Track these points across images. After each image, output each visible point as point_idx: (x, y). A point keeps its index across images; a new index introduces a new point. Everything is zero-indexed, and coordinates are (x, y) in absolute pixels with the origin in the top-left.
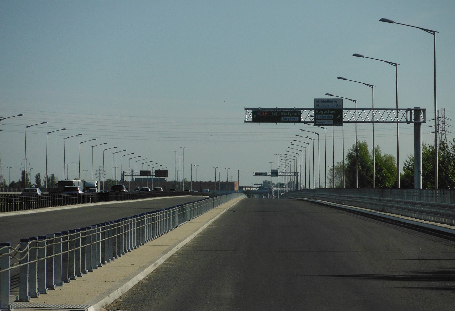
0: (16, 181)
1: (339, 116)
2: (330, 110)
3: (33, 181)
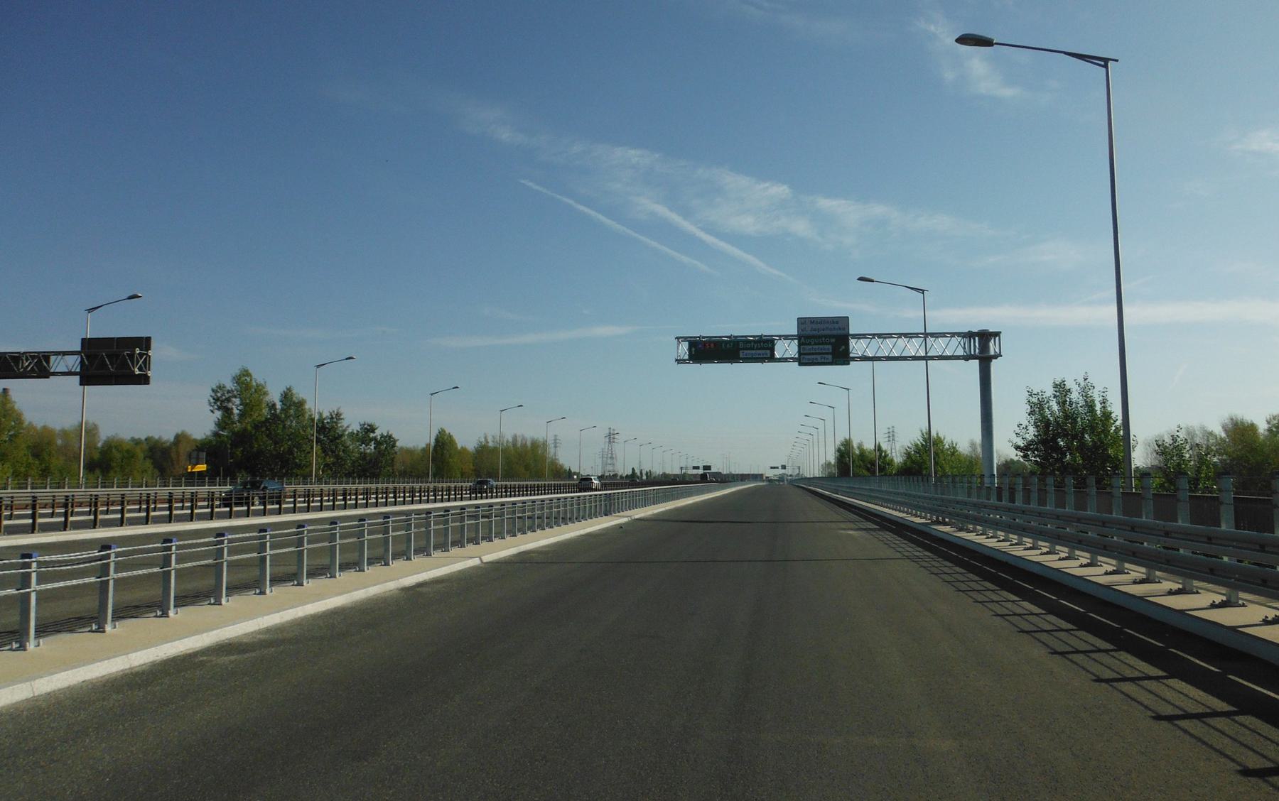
1: (843, 347)
2: (826, 337)
3: (639, 474)
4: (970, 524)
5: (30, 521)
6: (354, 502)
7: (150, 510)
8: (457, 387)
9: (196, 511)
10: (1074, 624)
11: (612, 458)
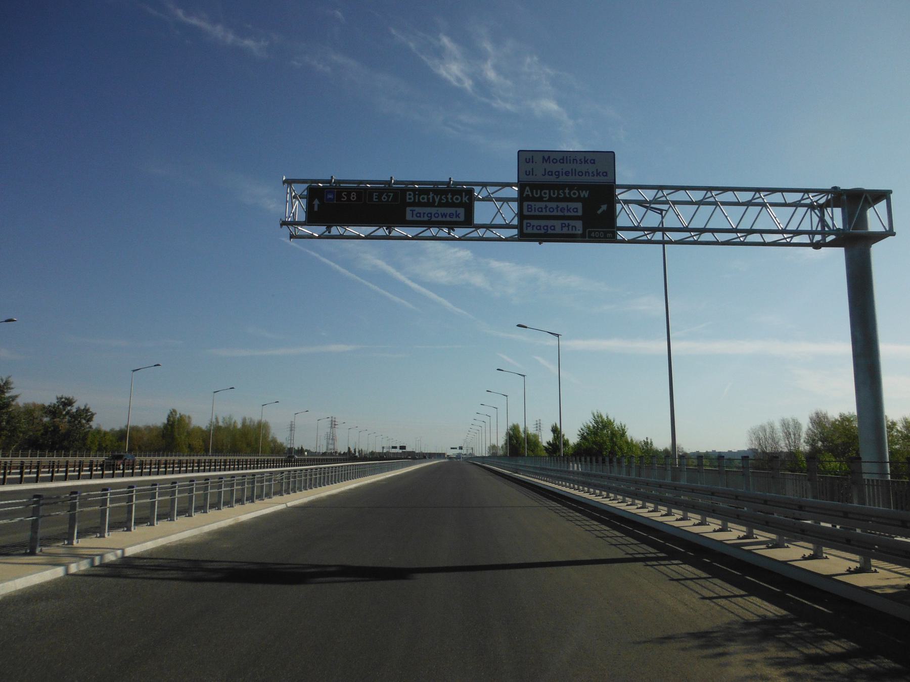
0: (346, 452)
1: (604, 207)
2: (571, 187)
3: (353, 452)
4: (592, 488)
5: (64, 474)
6: (185, 469)
7: (7, 474)
8: (233, 388)
9: (40, 475)
10: (657, 550)
11: (333, 439)
